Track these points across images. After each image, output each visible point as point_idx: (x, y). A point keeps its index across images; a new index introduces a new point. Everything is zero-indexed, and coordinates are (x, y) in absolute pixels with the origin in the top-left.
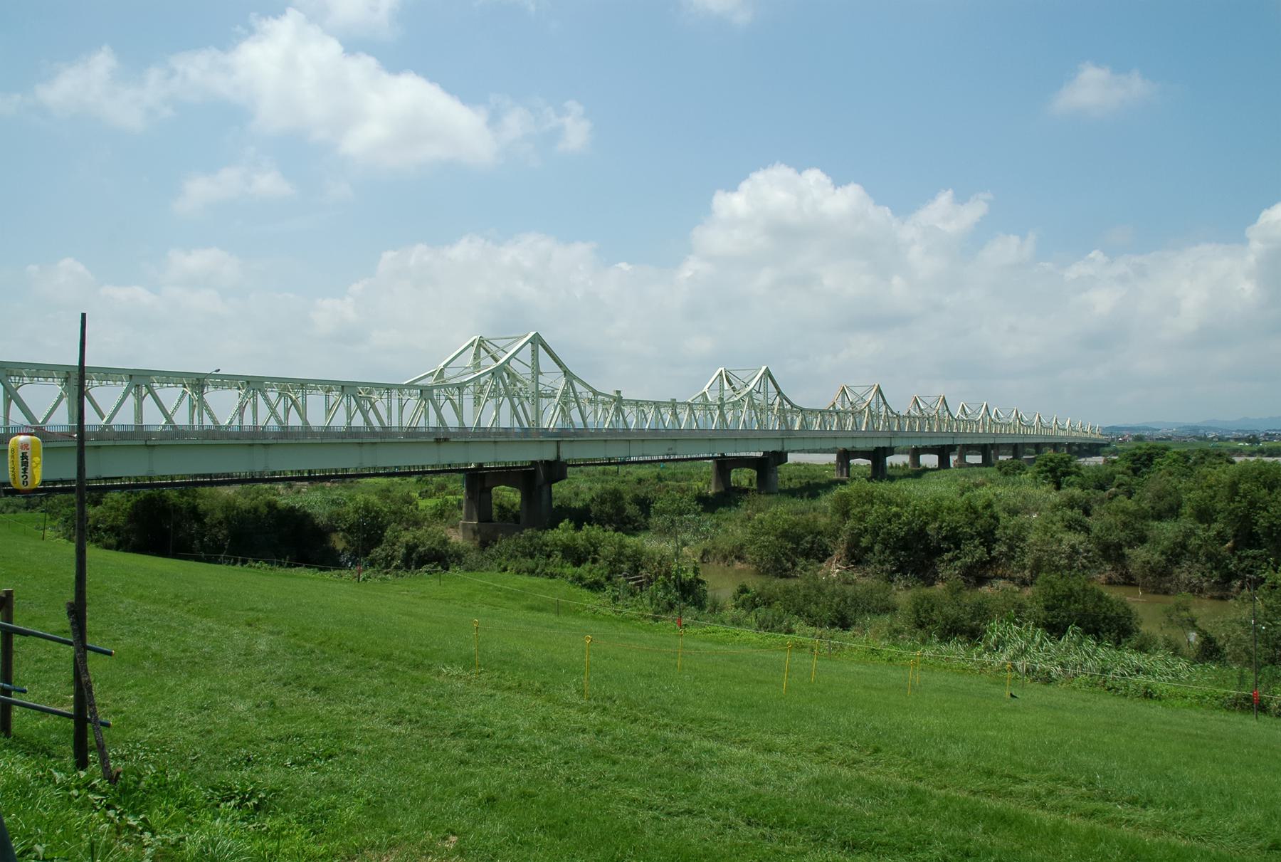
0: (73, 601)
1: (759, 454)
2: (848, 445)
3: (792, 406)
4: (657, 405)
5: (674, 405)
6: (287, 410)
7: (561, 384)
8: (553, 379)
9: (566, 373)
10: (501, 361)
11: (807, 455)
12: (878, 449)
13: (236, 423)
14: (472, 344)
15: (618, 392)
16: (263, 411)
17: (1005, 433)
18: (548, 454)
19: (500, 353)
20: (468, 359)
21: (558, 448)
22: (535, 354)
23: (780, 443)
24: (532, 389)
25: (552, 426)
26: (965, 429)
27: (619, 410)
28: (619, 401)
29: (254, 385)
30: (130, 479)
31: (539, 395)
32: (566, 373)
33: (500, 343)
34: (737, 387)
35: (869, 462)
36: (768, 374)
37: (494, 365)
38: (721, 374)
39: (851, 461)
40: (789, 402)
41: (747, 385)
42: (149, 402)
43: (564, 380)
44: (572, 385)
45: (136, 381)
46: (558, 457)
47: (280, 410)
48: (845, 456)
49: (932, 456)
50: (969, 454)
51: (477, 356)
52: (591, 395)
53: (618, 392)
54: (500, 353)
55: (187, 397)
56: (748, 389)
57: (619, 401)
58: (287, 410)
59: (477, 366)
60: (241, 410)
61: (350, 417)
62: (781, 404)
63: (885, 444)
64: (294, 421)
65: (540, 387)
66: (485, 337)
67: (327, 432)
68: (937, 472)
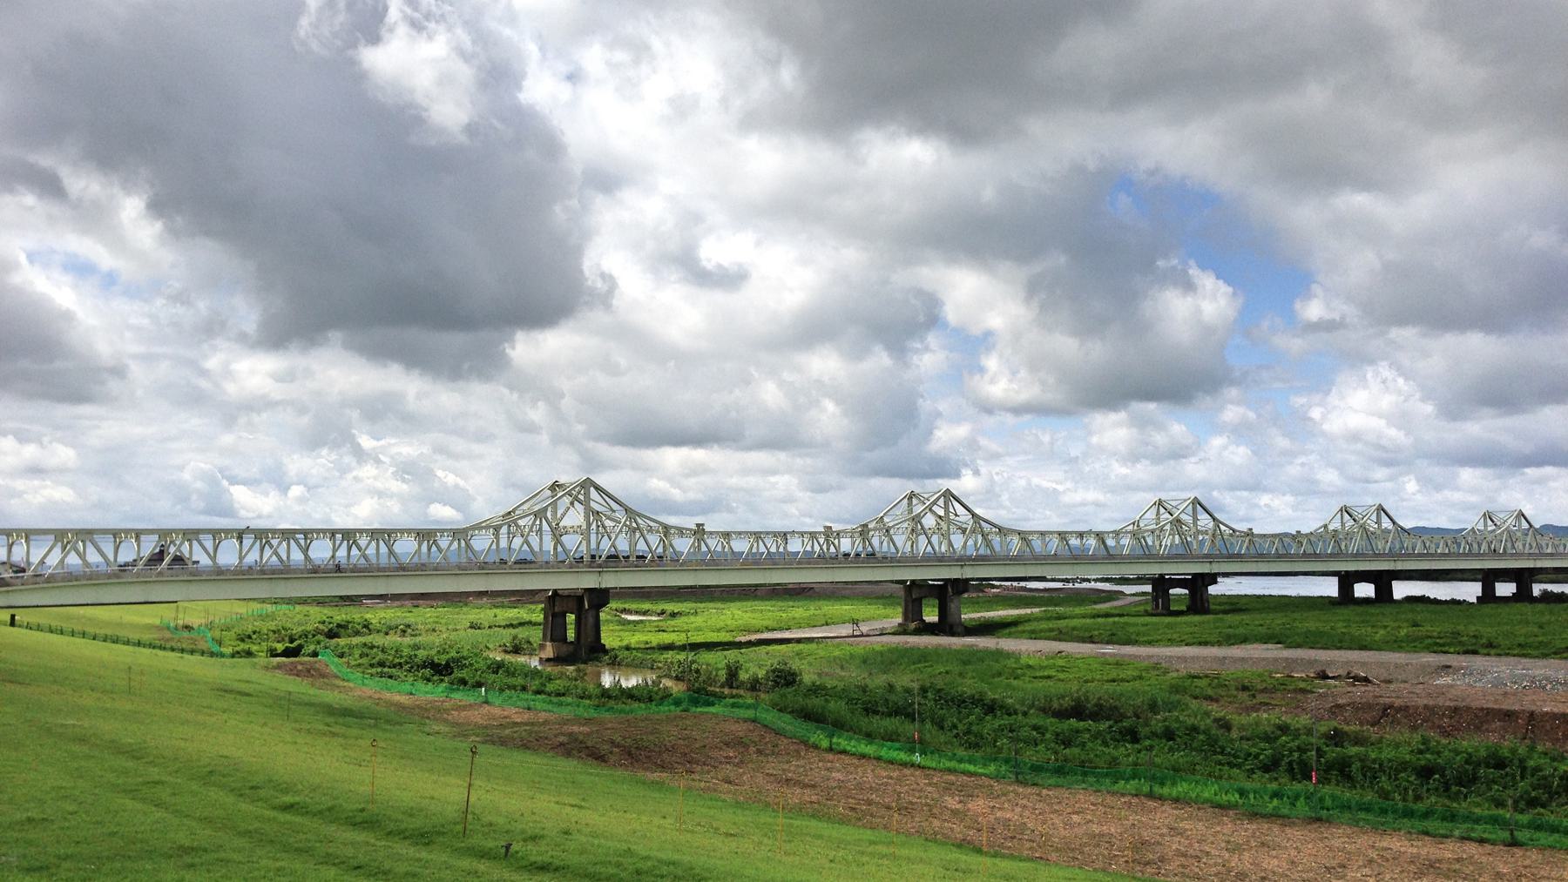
0: (1480, 595)
7: (1211, 524)
9: (1214, 519)
10: (1175, 516)
14: (1155, 504)
15: (1251, 529)
19: (1174, 510)
20: (1152, 515)
22: (1194, 510)
24: (1193, 530)
25: (1166, 553)
29: (758, 536)
32: (1214, 519)
33: (926, 496)
34: (1498, 523)
35: (1187, 591)
37: (1171, 518)
39: (1171, 591)
42: (374, 544)
44: (1218, 526)
49: (1393, 586)
50: (1498, 582)
51: (910, 504)
52: (1231, 532)
53: (1251, 529)
55: (720, 543)
56: (1507, 524)
60: (752, 546)
65: (1199, 527)
66: (1163, 499)
68: (1372, 610)
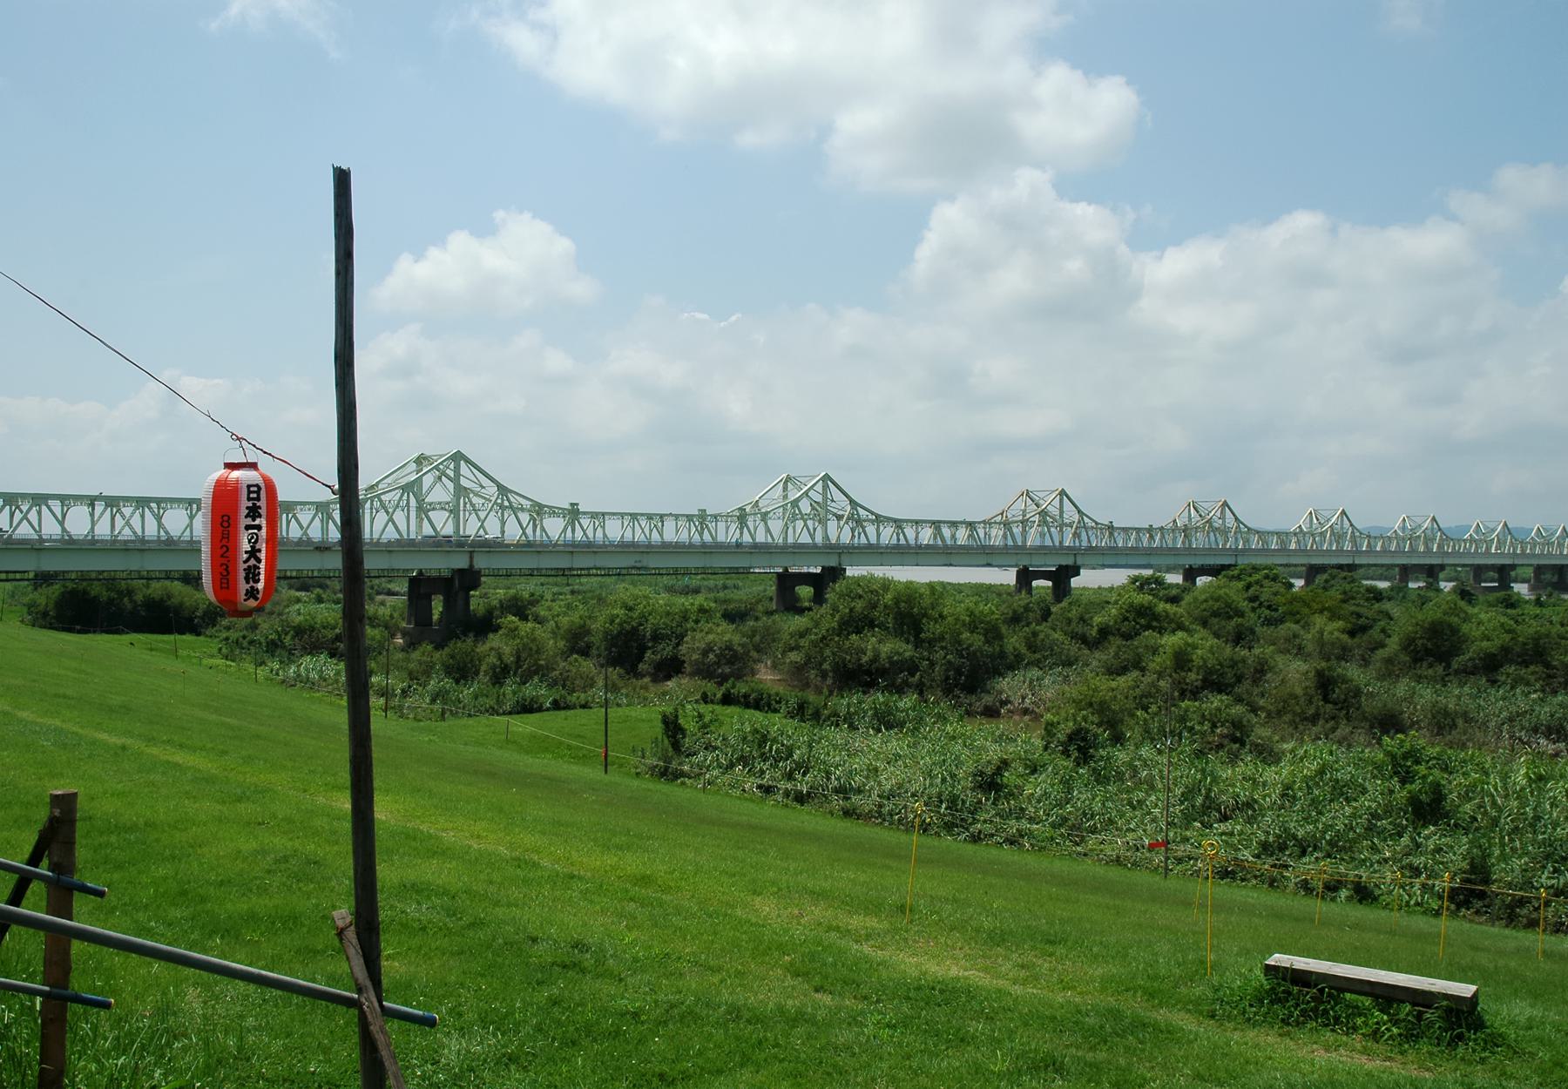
1: (819, 570)
2: (1197, 562)
3: (1249, 529)
4: (1138, 530)
5: (1150, 530)
6: (651, 531)
7: (1076, 517)
8: (1071, 515)
9: (1079, 511)
11: (1462, 563)
12: (1061, 568)
13: (562, 538)
16: (119, 522)
17: (1509, 553)
18: (461, 562)
21: (471, 558)
22: (1061, 501)
23: (1234, 558)
26: (1543, 551)
27: (1111, 534)
28: (1111, 528)
30: (398, 570)
31: (1062, 525)
32: (1079, 511)
36: (1343, 512)
38: (1311, 513)
40: (1246, 526)
41: (1329, 520)
43: (1077, 515)
45: (898, 523)
46: (471, 566)
47: (647, 531)
48: (1025, 576)
52: (1093, 524)
54: (1042, 502)
57: (1111, 528)
58: (651, 531)
59: (785, 497)
60: (565, 530)
61: (898, 540)
62: (1353, 532)
63: (1069, 561)
64: (655, 537)
66: (792, 475)
67: (677, 545)
